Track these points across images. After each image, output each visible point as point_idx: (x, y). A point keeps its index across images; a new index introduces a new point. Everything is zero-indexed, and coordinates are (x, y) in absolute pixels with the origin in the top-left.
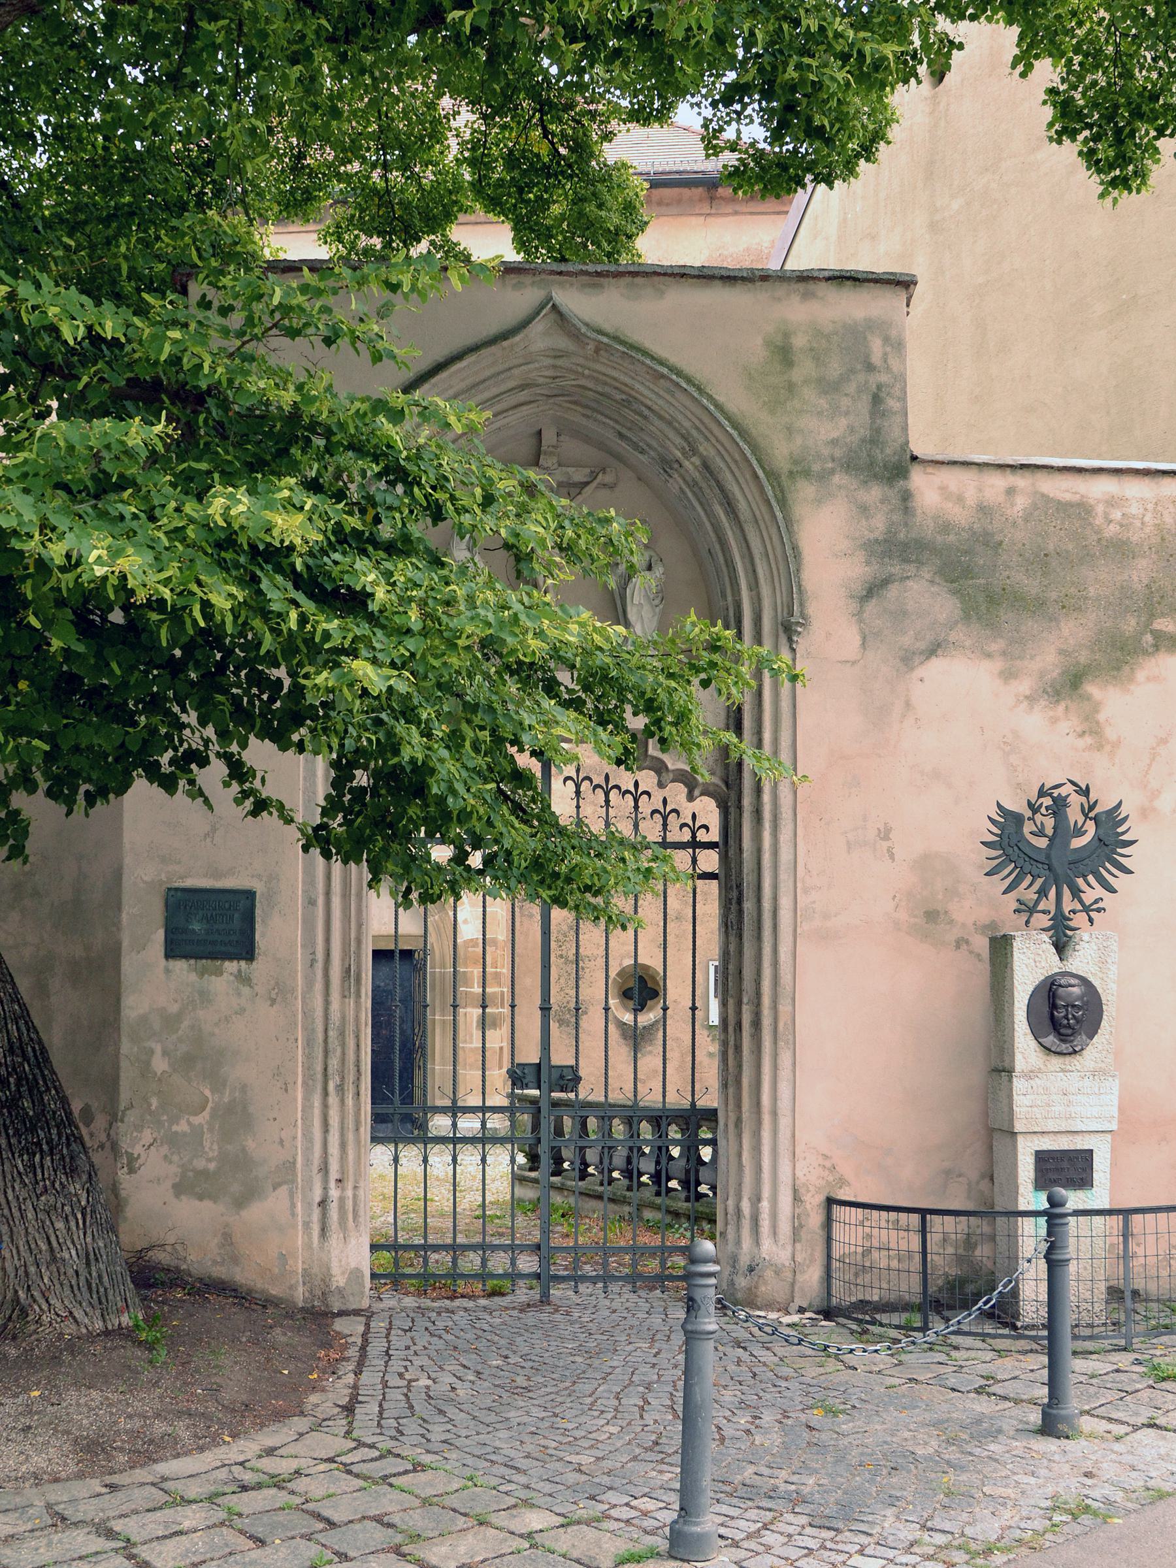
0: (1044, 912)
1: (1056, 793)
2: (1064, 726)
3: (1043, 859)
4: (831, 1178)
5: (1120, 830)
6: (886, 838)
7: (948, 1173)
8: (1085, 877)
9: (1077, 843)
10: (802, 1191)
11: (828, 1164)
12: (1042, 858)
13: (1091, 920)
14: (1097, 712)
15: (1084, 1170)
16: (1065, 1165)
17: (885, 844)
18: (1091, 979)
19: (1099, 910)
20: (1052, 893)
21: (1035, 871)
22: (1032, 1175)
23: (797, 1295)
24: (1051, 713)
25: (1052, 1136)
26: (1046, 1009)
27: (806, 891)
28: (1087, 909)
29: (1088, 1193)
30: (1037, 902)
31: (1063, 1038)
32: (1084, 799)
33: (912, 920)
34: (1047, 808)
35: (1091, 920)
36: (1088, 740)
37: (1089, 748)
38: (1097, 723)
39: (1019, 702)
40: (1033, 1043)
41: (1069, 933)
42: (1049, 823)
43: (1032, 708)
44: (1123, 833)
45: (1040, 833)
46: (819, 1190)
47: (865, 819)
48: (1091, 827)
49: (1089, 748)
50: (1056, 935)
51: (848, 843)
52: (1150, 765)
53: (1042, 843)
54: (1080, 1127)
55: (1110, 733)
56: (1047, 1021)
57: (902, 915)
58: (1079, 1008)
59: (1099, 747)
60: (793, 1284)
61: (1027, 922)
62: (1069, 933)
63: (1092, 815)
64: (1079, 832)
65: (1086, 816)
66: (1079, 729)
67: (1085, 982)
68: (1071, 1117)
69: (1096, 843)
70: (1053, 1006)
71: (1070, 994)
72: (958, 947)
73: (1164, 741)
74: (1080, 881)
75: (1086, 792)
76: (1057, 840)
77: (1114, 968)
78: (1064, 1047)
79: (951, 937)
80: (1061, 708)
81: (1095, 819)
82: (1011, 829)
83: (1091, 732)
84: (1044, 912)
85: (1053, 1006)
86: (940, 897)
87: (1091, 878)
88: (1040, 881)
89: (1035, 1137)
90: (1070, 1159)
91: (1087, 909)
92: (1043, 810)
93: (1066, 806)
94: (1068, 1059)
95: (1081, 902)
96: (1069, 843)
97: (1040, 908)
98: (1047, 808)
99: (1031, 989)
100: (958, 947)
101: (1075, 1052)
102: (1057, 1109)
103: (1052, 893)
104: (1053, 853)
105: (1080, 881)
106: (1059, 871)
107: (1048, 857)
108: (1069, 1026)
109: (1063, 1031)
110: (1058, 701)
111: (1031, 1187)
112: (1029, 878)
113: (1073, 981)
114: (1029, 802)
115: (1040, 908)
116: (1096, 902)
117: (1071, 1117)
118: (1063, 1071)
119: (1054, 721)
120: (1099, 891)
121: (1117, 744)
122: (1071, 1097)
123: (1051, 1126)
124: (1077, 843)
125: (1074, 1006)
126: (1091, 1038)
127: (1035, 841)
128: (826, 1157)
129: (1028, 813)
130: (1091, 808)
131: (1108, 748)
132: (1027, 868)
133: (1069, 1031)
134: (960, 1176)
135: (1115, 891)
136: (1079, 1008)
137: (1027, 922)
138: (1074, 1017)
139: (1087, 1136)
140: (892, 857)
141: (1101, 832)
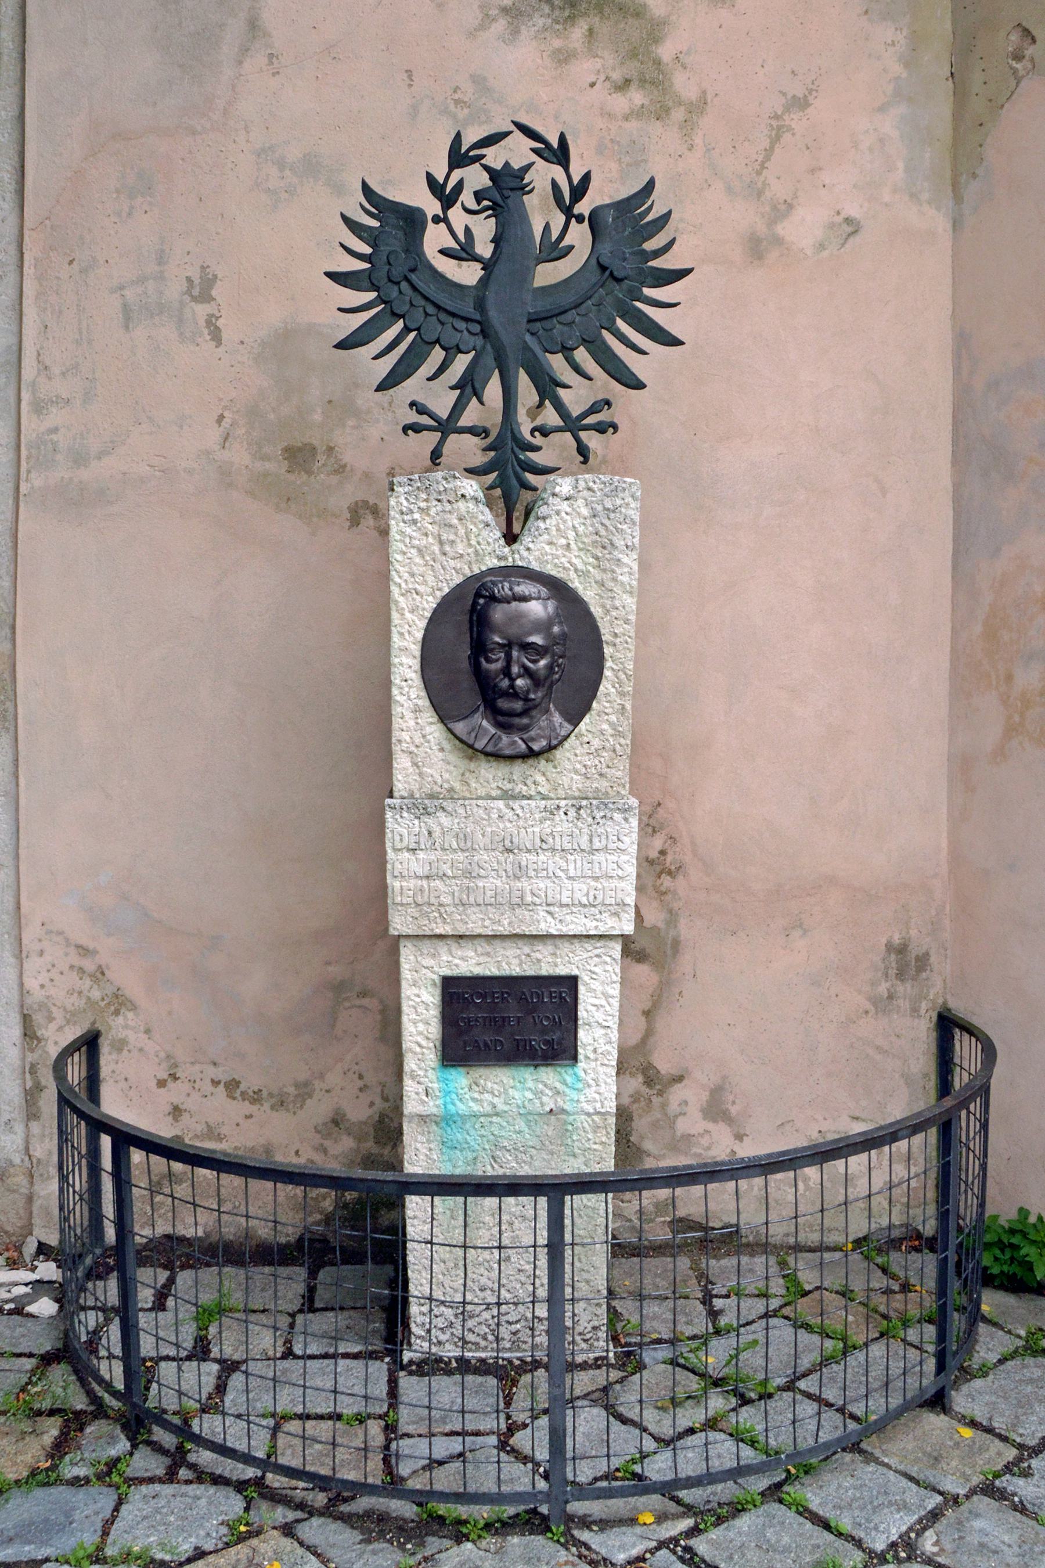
0: (472, 431)
1: (495, 157)
2: (585, 68)
3: (469, 310)
4: (96, 994)
5: (650, 245)
6: (206, 297)
7: (339, 988)
8: (567, 351)
9: (547, 274)
10: (38, 1018)
11: (89, 965)
12: (468, 309)
13: (583, 451)
14: (657, 41)
15: (557, 1024)
16: (513, 1012)
17: (202, 310)
18: (576, 584)
19: (601, 428)
20: (493, 390)
21: (451, 337)
22: (434, 1030)
23: (36, 1221)
24: (557, 43)
25: (483, 947)
26: (465, 652)
27: (39, 408)
28: (572, 425)
29: (567, 1074)
30: (458, 408)
31: (504, 721)
32: (557, 172)
33: (259, 466)
34: (479, 196)
35: (583, 451)
36: (637, 97)
37: (637, 113)
38: (658, 62)
39: (487, 20)
40: (435, 731)
41: (531, 478)
42: (484, 229)
43: (516, 32)
44: (658, 253)
45: (464, 252)
46: (71, 1017)
47: (161, 259)
48: (579, 236)
49: (637, 113)
50: (501, 482)
51: (126, 309)
52: (769, 152)
53: (468, 274)
54: (548, 925)
55: (686, 87)
56: (467, 682)
57: (239, 456)
58: (541, 651)
59: (661, 113)
60: (30, 1199)
61: (436, 455)
62: (531, 478)
63: (583, 207)
64: (555, 251)
65: (568, 213)
66: (617, 76)
67: (558, 589)
68: (522, 904)
69: (595, 276)
70: (479, 648)
71: (520, 616)
72: (355, 520)
73: (801, 103)
74: (557, 363)
75: (560, 154)
76: (500, 269)
77: (631, 560)
78: (508, 742)
79: (342, 499)
80: (578, 33)
81: (594, 220)
82: (394, 242)
83: (643, 81)
84: (472, 431)
85: (479, 648)
86: (317, 417)
87: (581, 355)
88: (461, 363)
89: (442, 948)
90: (522, 999)
91: (572, 425)
92: (467, 198)
93: (523, 189)
94: (518, 769)
95: (560, 407)
96: (527, 274)
97: (464, 421)
98: (479, 196)
99: (430, 604)
100: (355, 520)
101: (531, 754)
102: (492, 883)
103: (493, 390)
104: (491, 296)
105: (557, 363)
106: (506, 337)
107: (480, 305)
108: (513, 694)
109: (503, 704)
110: (572, 19)
111: (432, 1057)
112: (438, 354)
113: (525, 588)
114: (430, 179)
115: (464, 421)
116: (593, 410)
117: (522, 904)
118: (507, 796)
119: (563, 58)
120: (604, 384)
121: (699, 107)
122: (524, 858)
123: (475, 923)
124: (547, 274)
125: (526, 647)
126: (575, 718)
127: (447, 267)
128: (84, 951)
129: (432, 206)
130: (579, 191)
131: (678, 114)
132: (434, 328)
133: (518, 706)
134: (363, 994)
135: (639, 386)
136: (541, 651)
137: (436, 455)
138: (527, 672)
139: (565, 947)
140: (216, 336)
141: (606, 248)
